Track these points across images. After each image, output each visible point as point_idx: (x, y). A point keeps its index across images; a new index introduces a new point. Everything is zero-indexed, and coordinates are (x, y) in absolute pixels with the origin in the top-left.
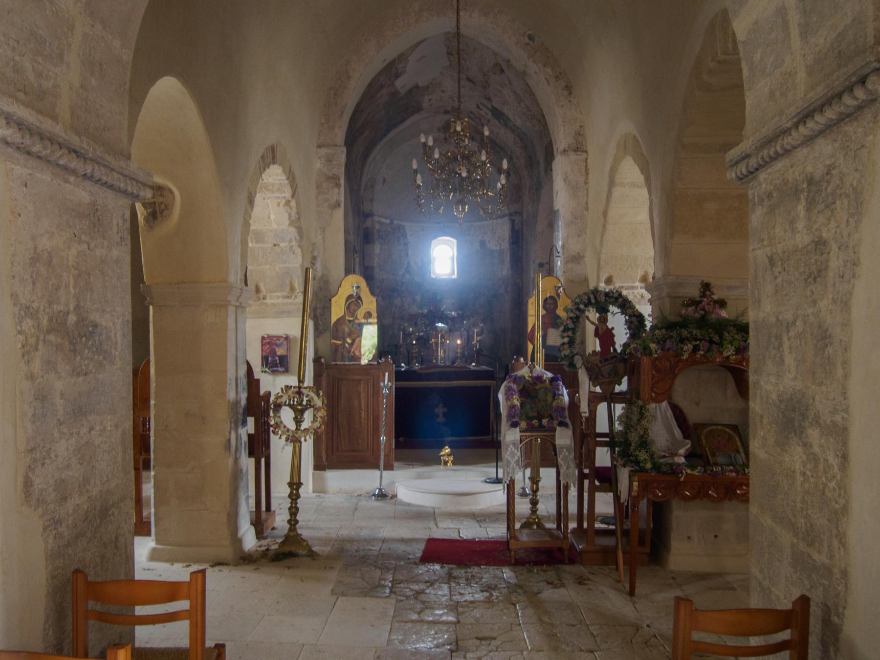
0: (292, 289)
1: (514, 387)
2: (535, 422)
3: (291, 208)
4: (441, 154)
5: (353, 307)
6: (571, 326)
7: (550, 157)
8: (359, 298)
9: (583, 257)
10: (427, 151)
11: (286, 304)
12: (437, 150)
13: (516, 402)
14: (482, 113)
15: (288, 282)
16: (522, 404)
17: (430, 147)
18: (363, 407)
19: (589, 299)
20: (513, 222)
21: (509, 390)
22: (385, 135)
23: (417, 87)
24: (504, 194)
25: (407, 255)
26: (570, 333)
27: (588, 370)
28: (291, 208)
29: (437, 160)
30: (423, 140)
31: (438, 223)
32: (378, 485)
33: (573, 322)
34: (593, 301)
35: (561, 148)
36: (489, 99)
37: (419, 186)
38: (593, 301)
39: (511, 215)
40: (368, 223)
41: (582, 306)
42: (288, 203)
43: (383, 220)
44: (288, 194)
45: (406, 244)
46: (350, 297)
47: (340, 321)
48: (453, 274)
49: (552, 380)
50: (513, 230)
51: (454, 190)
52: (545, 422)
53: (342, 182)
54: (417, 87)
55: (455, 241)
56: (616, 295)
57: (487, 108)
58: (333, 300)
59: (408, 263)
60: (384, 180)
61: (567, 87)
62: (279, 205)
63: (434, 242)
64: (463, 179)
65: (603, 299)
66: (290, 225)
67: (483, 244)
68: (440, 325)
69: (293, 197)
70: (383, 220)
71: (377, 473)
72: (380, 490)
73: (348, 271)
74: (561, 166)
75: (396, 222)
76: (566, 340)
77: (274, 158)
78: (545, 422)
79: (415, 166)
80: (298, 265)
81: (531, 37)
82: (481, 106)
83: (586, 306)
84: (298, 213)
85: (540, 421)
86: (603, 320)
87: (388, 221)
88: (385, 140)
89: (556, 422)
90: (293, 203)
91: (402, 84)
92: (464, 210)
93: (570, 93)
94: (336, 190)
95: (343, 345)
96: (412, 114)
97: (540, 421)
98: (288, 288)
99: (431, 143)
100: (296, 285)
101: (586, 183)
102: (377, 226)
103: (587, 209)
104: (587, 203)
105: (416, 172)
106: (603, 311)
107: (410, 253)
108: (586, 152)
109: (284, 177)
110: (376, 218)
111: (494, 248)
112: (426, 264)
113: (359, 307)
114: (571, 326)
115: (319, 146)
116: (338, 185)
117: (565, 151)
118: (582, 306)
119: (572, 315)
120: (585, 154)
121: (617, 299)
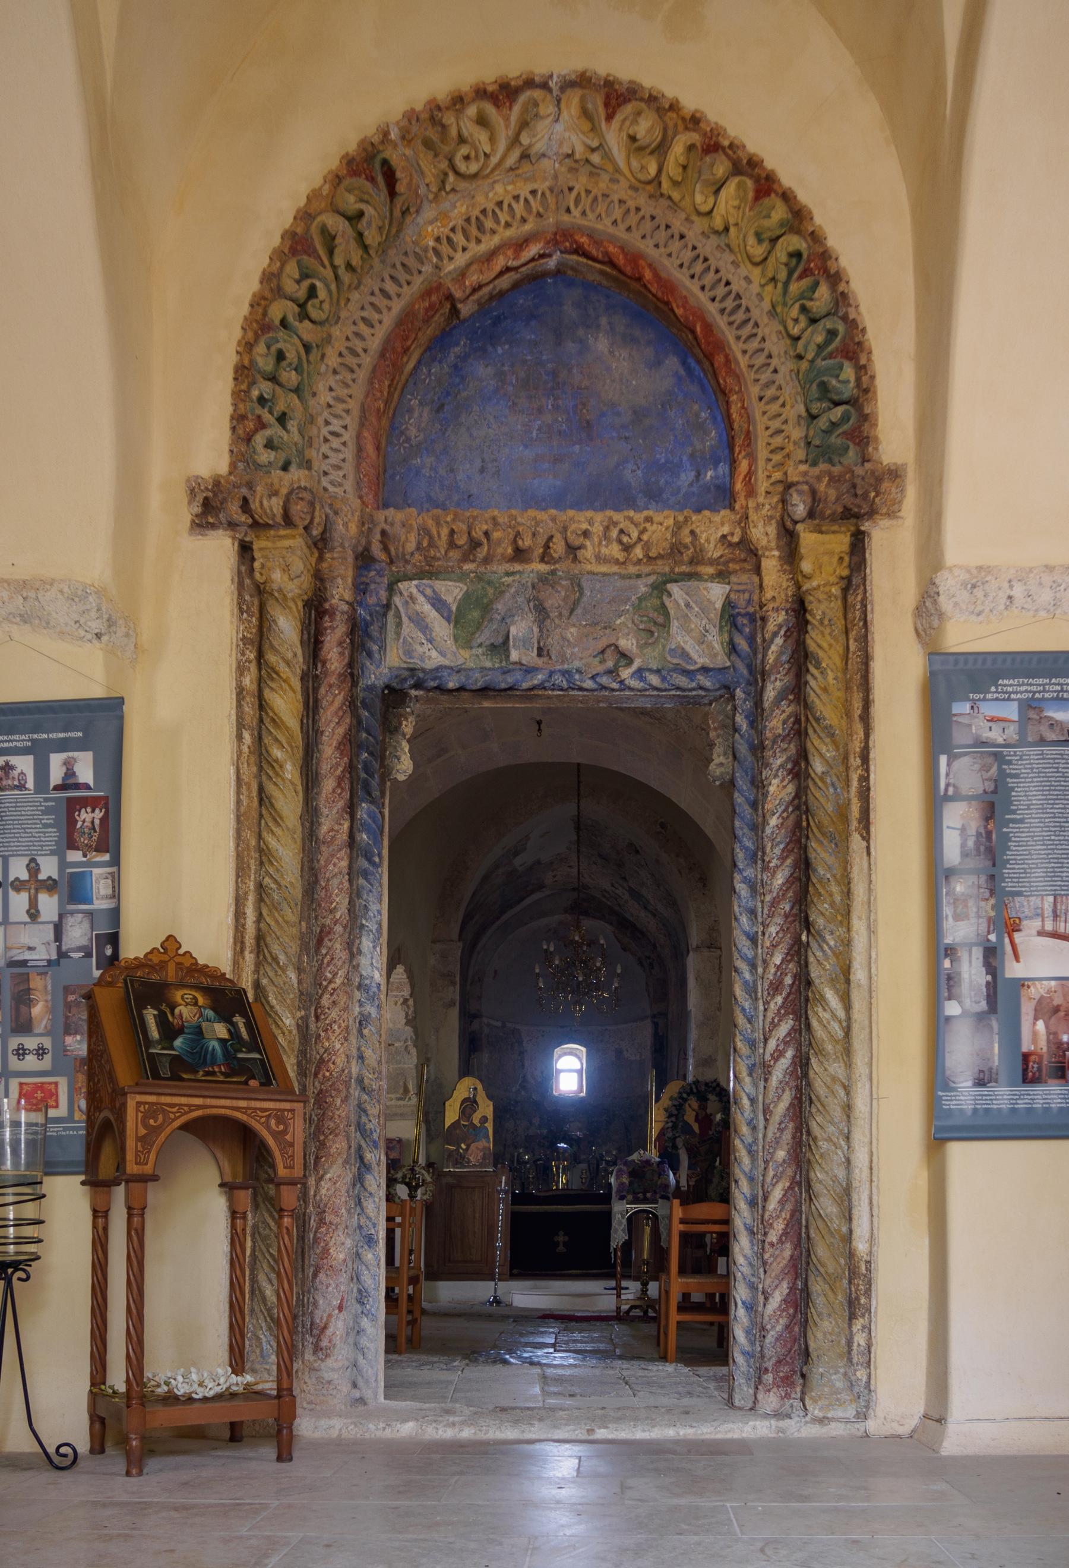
0: (406, 1090)
1: (625, 1168)
2: (640, 1196)
3: (408, 1007)
4: (561, 960)
5: (468, 1110)
6: (675, 1112)
7: (679, 954)
8: (476, 1102)
9: (715, 1060)
10: (548, 956)
11: (400, 1106)
12: (557, 957)
13: (625, 1180)
14: (617, 891)
15: (401, 1083)
16: (631, 1183)
17: (551, 953)
18: (477, 1215)
19: (691, 1089)
20: (656, 1024)
21: (620, 1171)
22: (498, 918)
23: (539, 862)
24: (53, 1130)
25: (523, 1066)
26: (673, 1119)
27: (687, 1150)
28: (408, 1007)
29: (557, 966)
30: (545, 947)
31: (562, 1027)
32: (493, 1293)
33: (677, 1110)
34: (695, 1090)
35: (694, 945)
36: (624, 878)
37: (541, 988)
38: (695, 1090)
39: (654, 1016)
40: (475, 1026)
41: (685, 1095)
42: (406, 1001)
43: (492, 1022)
44: (406, 992)
45: (521, 1053)
46: (465, 1100)
47: (455, 1125)
48: (582, 1091)
49: (659, 1163)
50: (656, 1034)
51: (572, 992)
52: (649, 1195)
53: (458, 979)
54: (539, 862)
55: (584, 1049)
56: (714, 1084)
57: (623, 888)
58: (447, 1103)
59: (524, 1077)
60: (496, 972)
61: (700, 879)
62: (396, 1004)
63: (557, 1051)
64: (580, 983)
65: (703, 1088)
66: (406, 1024)
67: (619, 1053)
68: (562, 1145)
69: (411, 995)
70: (492, 1022)
71: (493, 1283)
72: (495, 1297)
73: (466, 1070)
74: (692, 962)
75: (509, 1025)
76: (670, 1125)
77: (399, 958)
78: (649, 1195)
79: (537, 971)
80: (412, 1066)
81: (663, 826)
82: (616, 885)
83: (688, 1095)
84: (415, 1012)
85: (645, 1194)
86: (703, 1107)
87: (499, 1024)
88: (498, 923)
89: (658, 1196)
90: (411, 1002)
91: (520, 862)
92: (581, 1009)
93: (705, 885)
94: (451, 988)
95: (457, 1150)
96: (532, 892)
97: (645, 1194)
98: (401, 1091)
99: (552, 949)
100: (411, 1087)
101: (719, 982)
102: (486, 1030)
103: (719, 1009)
104: (720, 1003)
105: (538, 975)
106: (703, 1099)
107: (527, 1063)
108: (720, 948)
109: (405, 976)
110: (485, 1020)
111: (633, 1058)
112: (548, 1077)
113: (475, 1111)
114: (675, 1112)
115: (433, 942)
116: (453, 983)
117: (698, 947)
118: (685, 1095)
119: (676, 1103)
120: (719, 951)
121: (714, 1089)
